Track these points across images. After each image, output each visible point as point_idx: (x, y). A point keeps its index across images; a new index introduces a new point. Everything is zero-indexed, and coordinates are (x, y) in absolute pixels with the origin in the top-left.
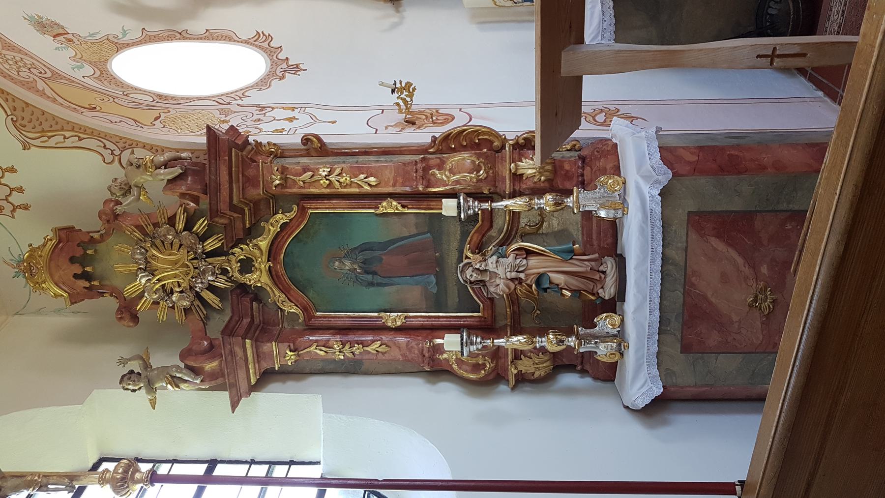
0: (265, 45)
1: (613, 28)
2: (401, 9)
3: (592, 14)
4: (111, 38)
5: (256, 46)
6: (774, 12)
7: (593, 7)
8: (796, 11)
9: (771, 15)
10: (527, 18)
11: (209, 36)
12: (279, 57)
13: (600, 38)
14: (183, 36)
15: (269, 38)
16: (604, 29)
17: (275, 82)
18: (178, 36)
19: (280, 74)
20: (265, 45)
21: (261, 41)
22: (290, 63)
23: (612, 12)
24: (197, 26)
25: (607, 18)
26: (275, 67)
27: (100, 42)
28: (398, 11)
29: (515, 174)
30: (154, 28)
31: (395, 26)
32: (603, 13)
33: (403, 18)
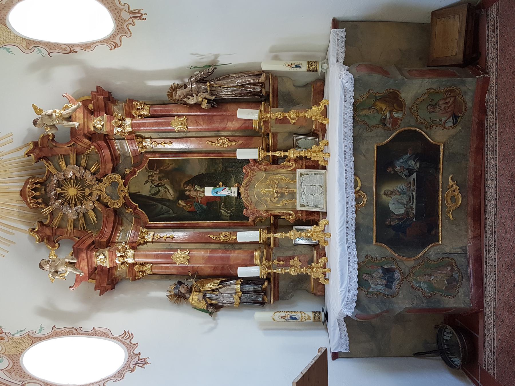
0: (128, 341)
1: (348, 343)
2: (216, 318)
3: (334, 334)
4: (31, 334)
5: (122, 342)
6: (448, 338)
7: (334, 330)
8: (463, 345)
9: (446, 340)
10: (294, 327)
11: (95, 333)
12: (135, 352)
13: (340, 348)
14: (77, 332)
15: (131, 336)
16: (342, 343)
17: (128, 374)
18: (75, 331)
19: (132, 367)
20: (128, 341)
21: (126, 340)
22: (141, 358)
23: (346, 333)
24: (88, 325)
25: (343, 337)
26: (130, 360)
27: (23, 337)
28: (214, 319)
29: (265, 294)
30: (61, 325)
31: (212, 329)
32: (341, 334)
33: (217, 324)
